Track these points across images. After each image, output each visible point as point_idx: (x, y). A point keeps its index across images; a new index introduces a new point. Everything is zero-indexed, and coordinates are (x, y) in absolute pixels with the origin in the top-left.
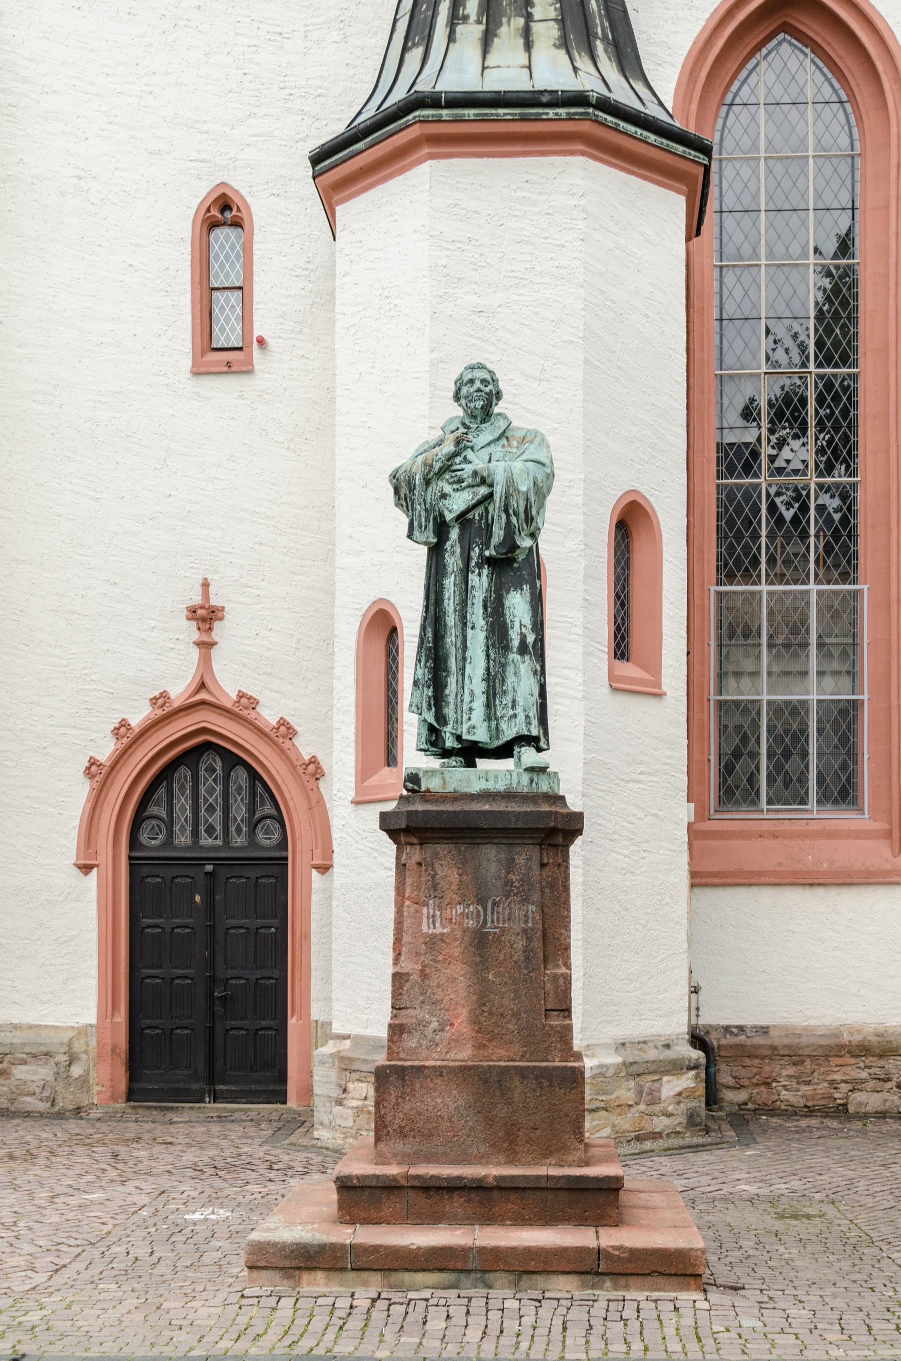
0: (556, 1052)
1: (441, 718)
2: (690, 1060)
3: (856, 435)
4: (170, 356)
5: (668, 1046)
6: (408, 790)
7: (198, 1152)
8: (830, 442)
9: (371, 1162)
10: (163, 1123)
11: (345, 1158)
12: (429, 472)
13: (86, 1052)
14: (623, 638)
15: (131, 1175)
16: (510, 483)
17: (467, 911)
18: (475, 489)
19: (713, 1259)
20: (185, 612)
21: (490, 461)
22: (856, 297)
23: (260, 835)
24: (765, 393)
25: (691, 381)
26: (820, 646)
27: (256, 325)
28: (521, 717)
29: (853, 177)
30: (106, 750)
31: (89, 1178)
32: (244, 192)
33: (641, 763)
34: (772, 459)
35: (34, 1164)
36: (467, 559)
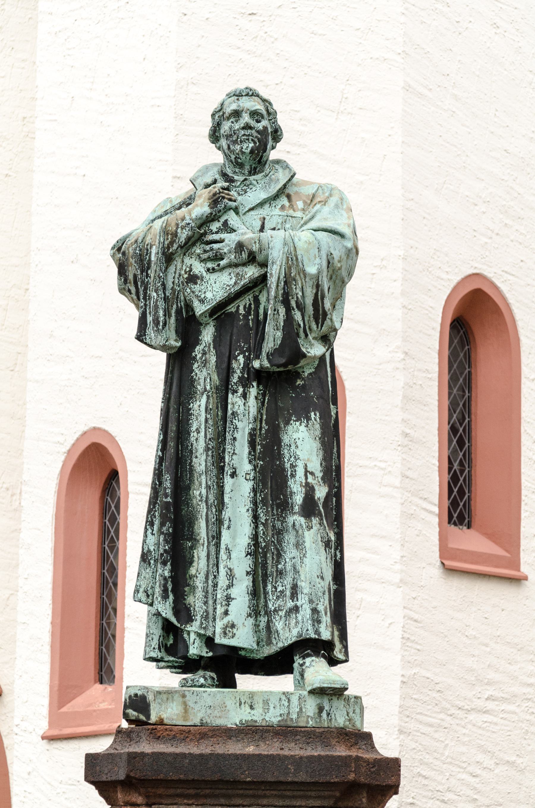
1: (183, 611)
12: (172, 243)
14: (461, 493)
18: (239, 270)
28: (306, 612)
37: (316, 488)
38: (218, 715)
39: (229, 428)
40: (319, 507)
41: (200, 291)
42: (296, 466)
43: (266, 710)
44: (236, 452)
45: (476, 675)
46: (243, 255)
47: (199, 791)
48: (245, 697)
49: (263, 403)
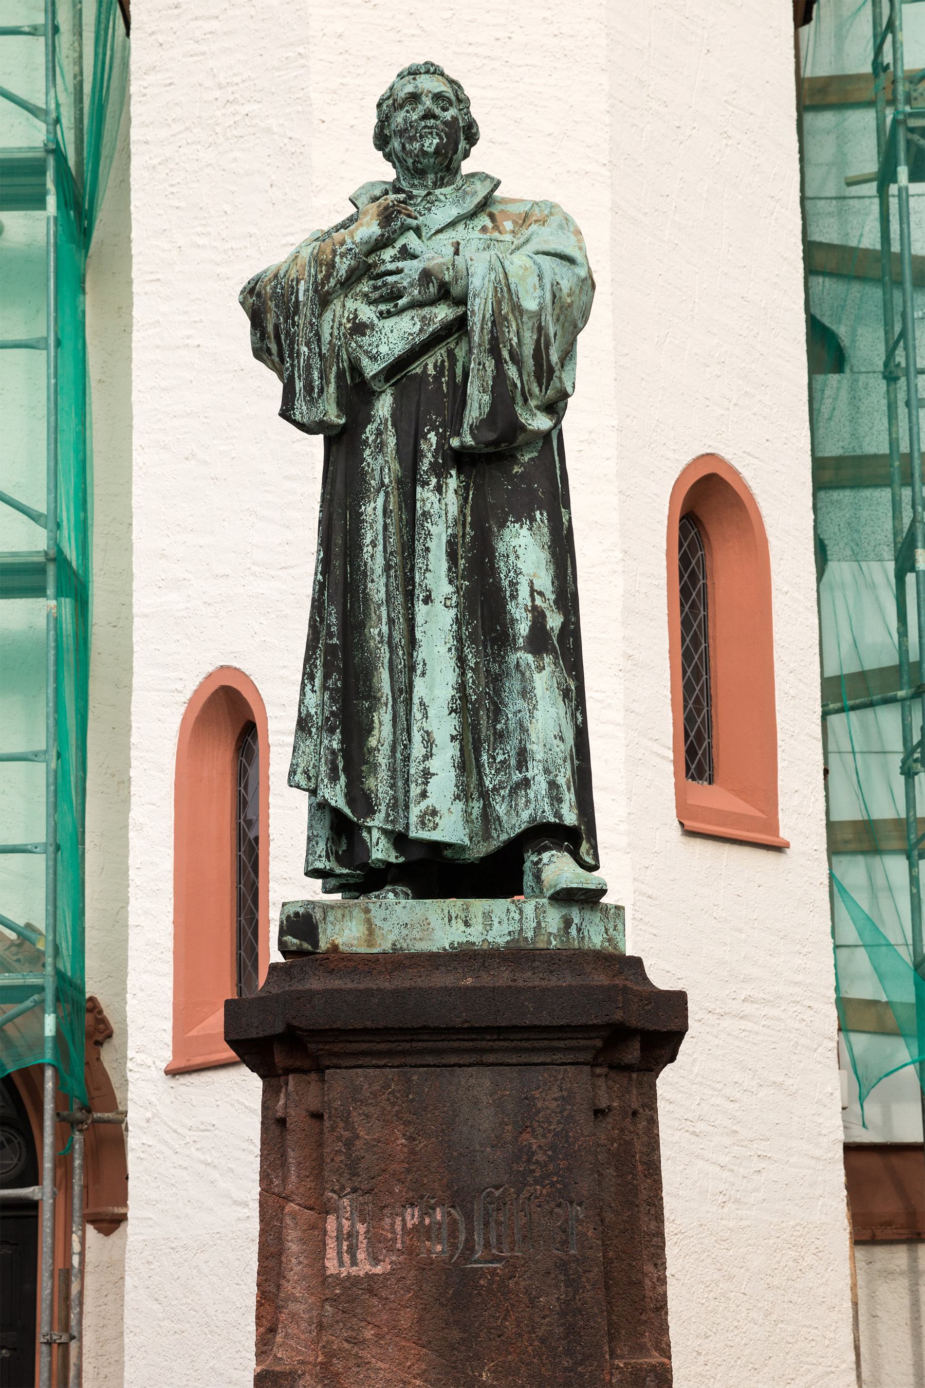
1: (361, 800)
12: (328, 276)
14: (699, 737)
17: (427, 1221)
18: (426, 311)
28: (540, 785)
37: (548, 613)
38: (418, 937)
39: (419, 534)
40: (552, 640)
41: (370, 345)
42: (518, 583)
43: (488, 926)
44: (430, 567)
45: (728, 969)
46: (431, 289)
47: (394, 1045)
48: (457, 909)
49: (466, 499)
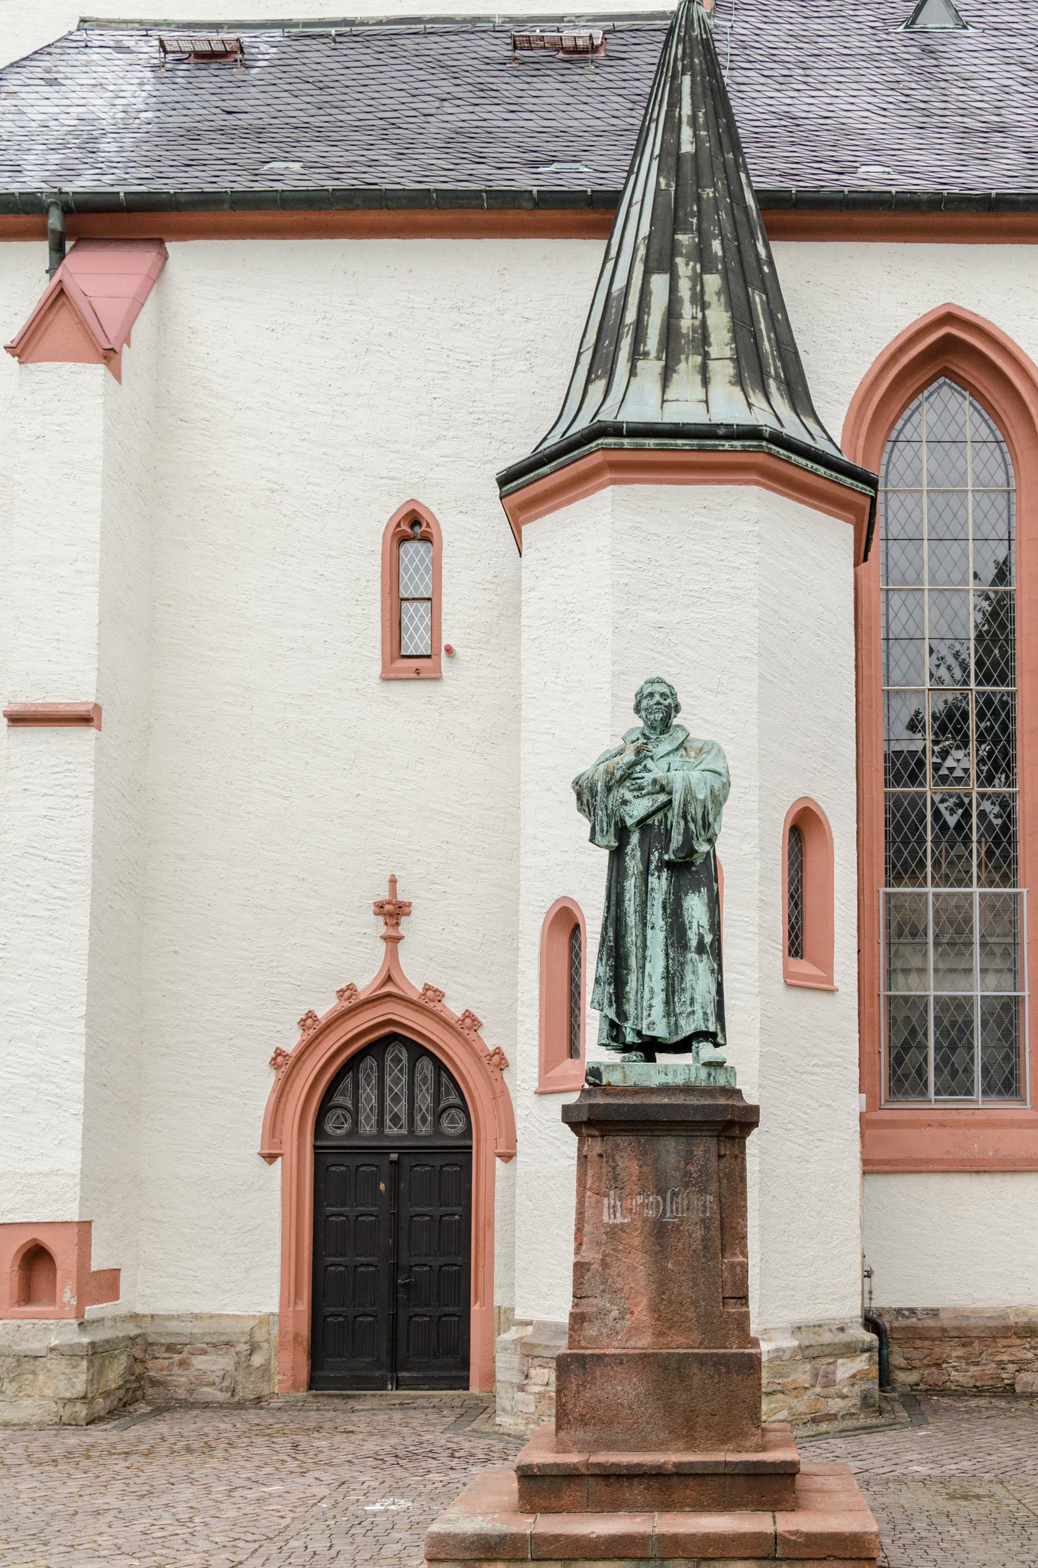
0: (733, 1339)
1: (622, 1014)
2: (863, 1343)
3: (1014, 748)
4: (360, 662)
5: (842, 1329)
6: (590, 1084)
7: (380, 1441)
8: (991, 753)
9: (552, 1451)
10: (344, 1412)
11: (528, 1444)
12: (611, 779)
13: (267, 1341)
14: (797, 936)
15: (311, 1466)
16: (688, 790)
18: (654, 796)
19: (886, 1541)
20: (373, 907)
21: (669, 770)
22: (1013, 621)
23: (445, 1124)
24: (930, 707)
25: (860, 695)
26: (983, 945)
27: (444, 635)
28: (699, 1014)
29: (1009, 511)
30: (292, 1041)
31: (268, 1470)
32: (433, 509)
33: (815, 1056)
34: (937, 767)
35: (212, 1457)
36: (647, 863)
